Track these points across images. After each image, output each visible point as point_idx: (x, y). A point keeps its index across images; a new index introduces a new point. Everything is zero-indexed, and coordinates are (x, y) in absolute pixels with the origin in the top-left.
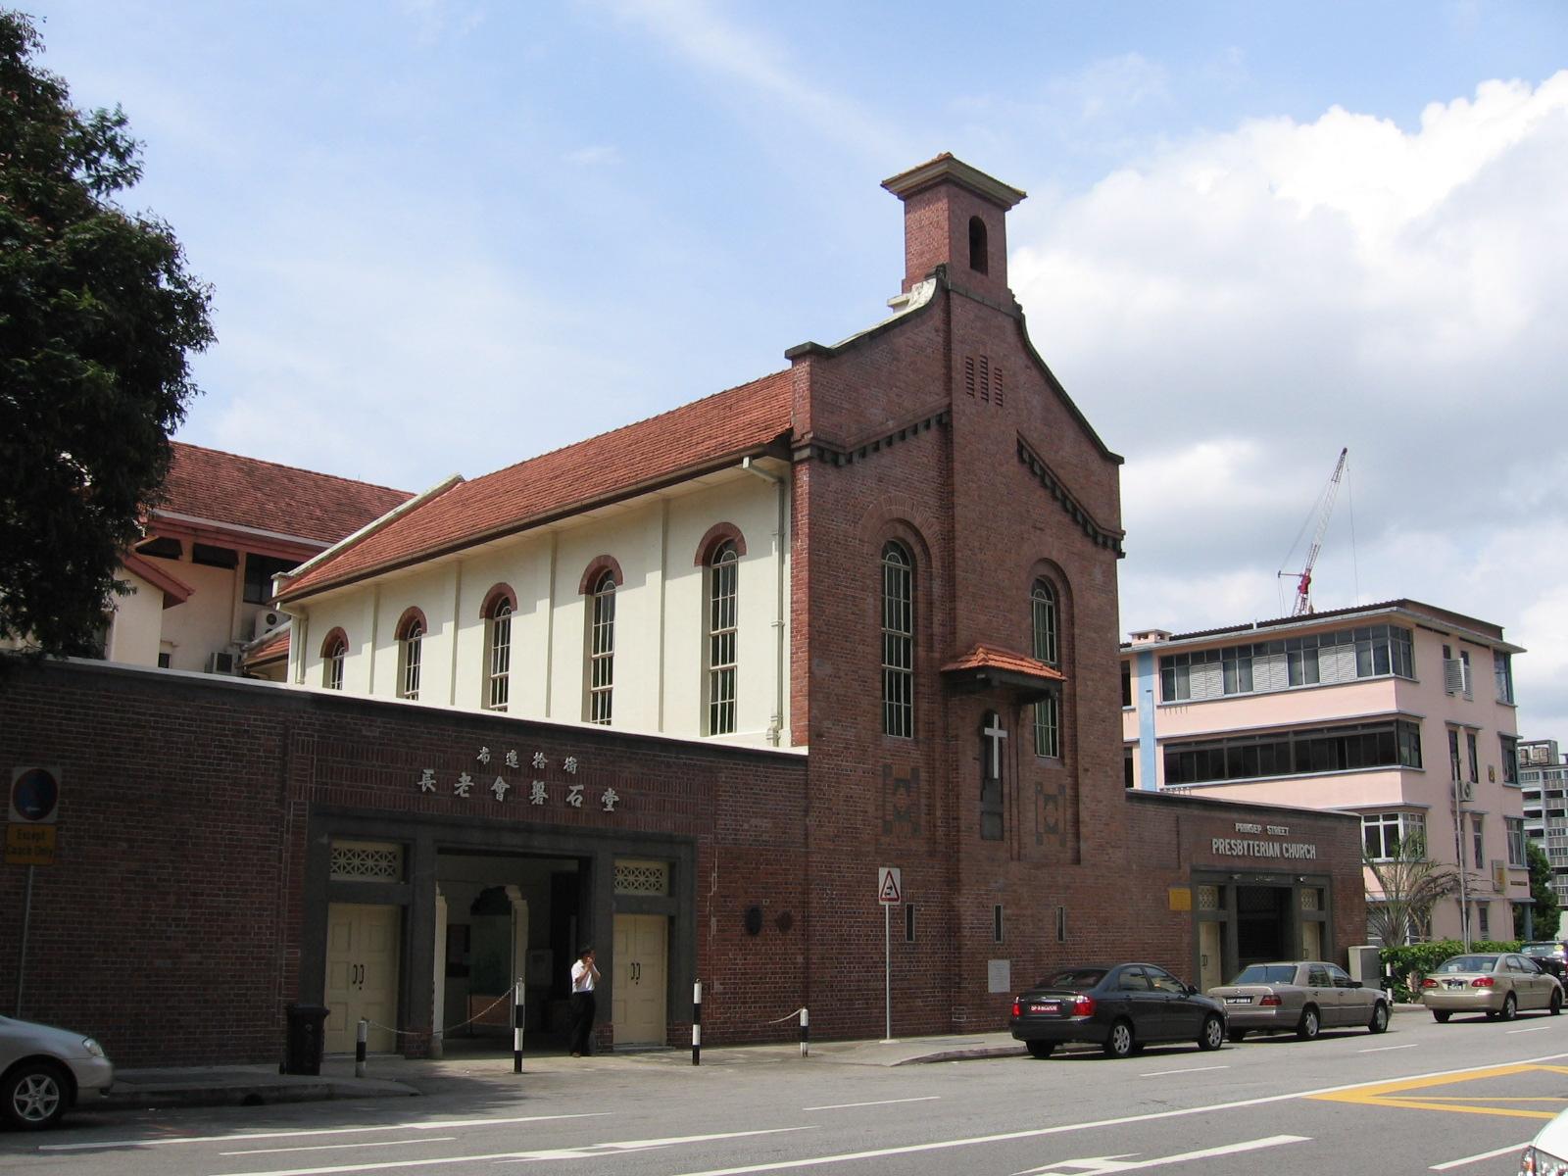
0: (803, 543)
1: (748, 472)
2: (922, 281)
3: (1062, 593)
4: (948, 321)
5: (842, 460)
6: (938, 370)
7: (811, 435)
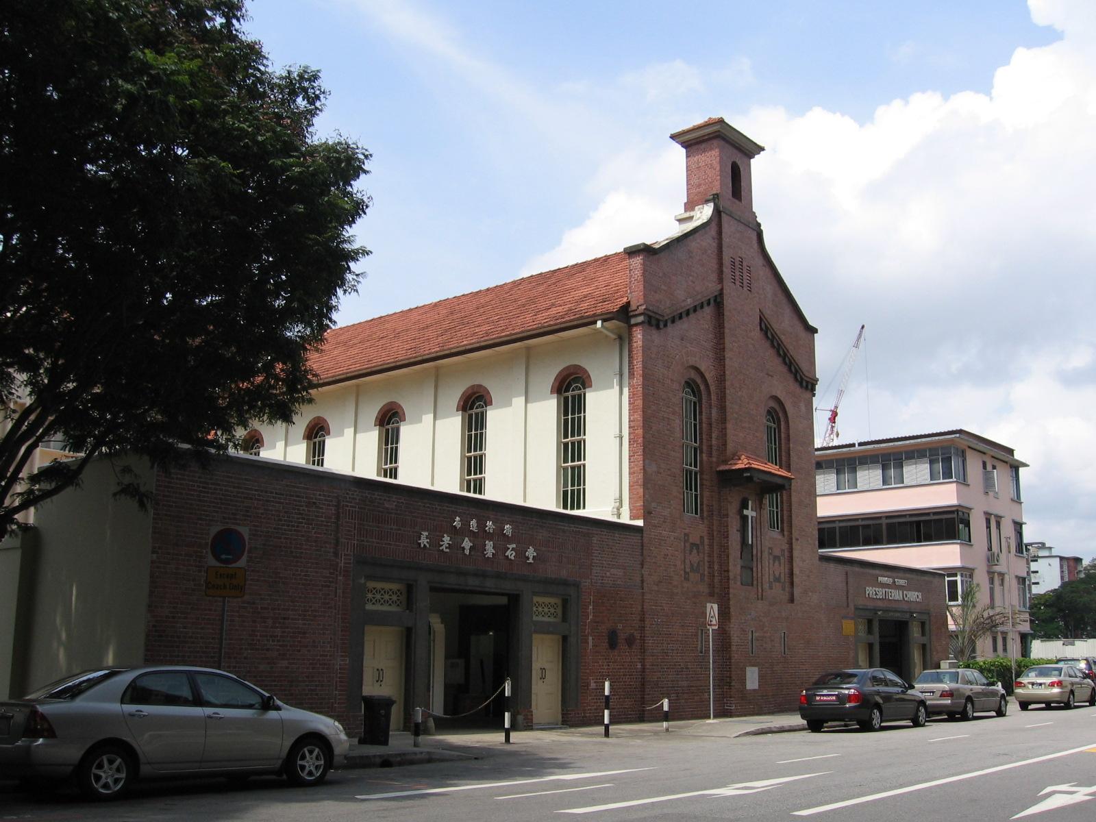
0: (638, 380)
1: (601, 332)
2: (703, 204)
3: (782, 419)
4: (720, 233)
5: (662, 325)
6: (713, 264)
7: (644, 307)
